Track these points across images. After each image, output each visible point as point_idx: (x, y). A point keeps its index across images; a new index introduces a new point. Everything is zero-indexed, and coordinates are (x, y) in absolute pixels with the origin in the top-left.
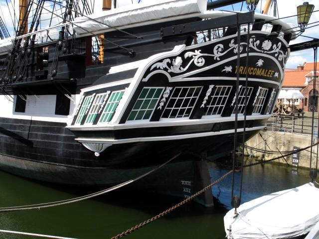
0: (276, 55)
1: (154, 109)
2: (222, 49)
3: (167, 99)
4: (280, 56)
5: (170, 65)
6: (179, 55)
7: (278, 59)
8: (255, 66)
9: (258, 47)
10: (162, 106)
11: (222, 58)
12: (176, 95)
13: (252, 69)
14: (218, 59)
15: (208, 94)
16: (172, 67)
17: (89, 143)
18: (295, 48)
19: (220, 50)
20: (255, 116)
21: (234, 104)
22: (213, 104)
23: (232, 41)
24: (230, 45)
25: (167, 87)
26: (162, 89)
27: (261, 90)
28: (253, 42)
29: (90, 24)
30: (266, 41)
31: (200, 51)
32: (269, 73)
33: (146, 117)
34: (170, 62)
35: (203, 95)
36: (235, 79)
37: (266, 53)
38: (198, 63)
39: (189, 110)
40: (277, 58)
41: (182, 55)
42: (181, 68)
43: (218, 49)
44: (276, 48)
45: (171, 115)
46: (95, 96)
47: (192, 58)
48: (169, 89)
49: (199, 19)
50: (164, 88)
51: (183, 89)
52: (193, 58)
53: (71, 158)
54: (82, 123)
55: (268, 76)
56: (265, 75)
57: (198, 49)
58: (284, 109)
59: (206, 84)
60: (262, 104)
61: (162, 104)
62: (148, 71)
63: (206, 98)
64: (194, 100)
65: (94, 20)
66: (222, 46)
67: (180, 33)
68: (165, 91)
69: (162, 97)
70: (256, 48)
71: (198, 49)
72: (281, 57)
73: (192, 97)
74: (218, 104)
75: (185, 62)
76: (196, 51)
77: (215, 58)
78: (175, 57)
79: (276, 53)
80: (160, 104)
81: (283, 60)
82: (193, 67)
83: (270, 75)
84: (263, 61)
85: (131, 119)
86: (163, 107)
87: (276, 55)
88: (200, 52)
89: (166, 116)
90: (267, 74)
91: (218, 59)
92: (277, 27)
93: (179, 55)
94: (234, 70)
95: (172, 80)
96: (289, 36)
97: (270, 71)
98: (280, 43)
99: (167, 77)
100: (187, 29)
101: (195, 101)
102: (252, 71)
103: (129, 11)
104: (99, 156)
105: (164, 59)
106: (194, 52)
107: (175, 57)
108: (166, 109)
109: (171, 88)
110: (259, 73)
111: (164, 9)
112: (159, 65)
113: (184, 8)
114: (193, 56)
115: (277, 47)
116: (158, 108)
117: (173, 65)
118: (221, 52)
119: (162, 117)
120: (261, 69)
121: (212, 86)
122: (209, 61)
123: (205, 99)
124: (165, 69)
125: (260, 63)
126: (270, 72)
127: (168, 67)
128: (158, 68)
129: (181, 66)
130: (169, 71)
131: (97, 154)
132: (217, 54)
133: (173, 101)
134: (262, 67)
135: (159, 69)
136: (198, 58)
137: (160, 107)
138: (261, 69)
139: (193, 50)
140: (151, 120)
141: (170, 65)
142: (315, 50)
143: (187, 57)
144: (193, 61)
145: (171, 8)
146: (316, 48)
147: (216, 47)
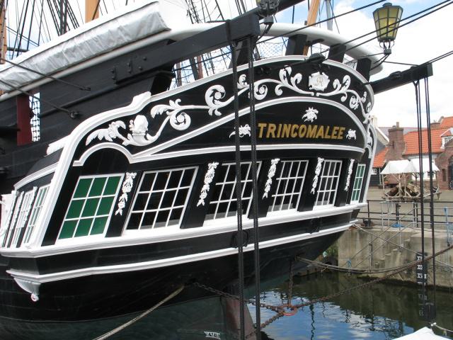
0: (343, 99)
1: (110, 215)
2: (222, 94)
3: (131, 195)
4: (352, 100)
5: (125, 132)
6: (142, 113)
7: (349, 107)
8: (300, 121)
9: (299, 86)
10: (204, 199)
11: (225, 111)
12: (146, 186)
13: (295, 126)
14: (218, 113)
15: (272, 173)
16: (129, 135)
17: (28, 281)
18: (380, 86)
19: (218, 96)
20: (322, 209)
21: (316, 189)
22: (281, 191)
23: (242, 78)
24: (239, 86)
25: (127, 174)
26: (120, 177)
27: (323, 164)
28: (288, 77)
29: (15, 73)
30: (316, 75)
31: (179, 100)
32: (334, 132)
33: (98, 229)
34: (124, 126)
35: (200, 183)
36: (260, 147)
37: (320, 97)
38: (178, 123)
39: (295, 197)
40: (347, 104)
41: (146, 111)
42: (148, 136)
43: (213, 95)
44: (340, 86)
45: (142, 225)
46: (24, 195)
47: (164, 115)
48: (131, 176)
49: (170, 41)
50: (122, 175)
51: (173, 172)
52: (167, 116)
53: (3, 305)
54: (19, 245)
55: (334, 137)
56: (327, 137)
57: (174, 98)
58: (408, 190)
59: (203, 161)
60: (334, 188)
61: (122, 205)
62: (81, 147)
63: (269, 181)
64: (183, 194)
65: (17, 65)
66: (221, 88)
67: (140, 72)
68: (124, 180)
69: (121, 193)
70: (295, 88)
71: (174, 98)
72: (354, 103)
73: (179, 188)
74: (289, 191)
75: (154, 124)
76: (171, 102)
77: (210, 113)
78: (133, 117)
79: (343, 95)
80: (119, 205)
81: (360, 106)
82: (170, 133)
83: (336, 135)
84: (317, 112)
85: (67, 234)
86: (126, 210)
87: (343, 99)
88: (180, 104)
89: (133, 225)
90: (330, 133)
91: (218, 113)
92: (338, 49)
93: (142, 113)
94: (255, 130)
95: (133, 159)
96: (366, 64)
97: (336, 128)
98: (347, 78)
99: (121, 153)
100: (156, 61)
101: (301, 183)
102: (296, 131)
103: (62, 43)
104: (37, 301)
105: (110, 122)
106: (168, 104)
107: (133, 117)
108: (132, 214)
109: (134, 175)
110: (312, 132)
111: (110, 32)
112: (101, 133)
113: (141, 25)
114: (167, 112)
115: (343, 85)
116: (117, 212)
117: (131, 133)
118: (221, 100)
119: (127, 229)
120: (316, 127)
121: (275, 161)
122: (200, 118)
123: (267, 183)
124: (117, 141)
125: (311, 114)
126: (338, 131)
127: (121, 136)
128: (100, 139)
129: (147, 132)
130: (126, 142)
131: (35, 297)
132: (213, 104)
133: (142, 199)
134: (316, 122)
135: (104, 140)
136: (177, 116)
137: (120, 211)
138: (316, 127)
139: (165, 101)
140: (108, 235)
141: (125, 132)
142: (416, 85)
143: (156, 115)
144: (169, 121)
145: (120, 29)
146: (418, 82)
147: (209, 92)
